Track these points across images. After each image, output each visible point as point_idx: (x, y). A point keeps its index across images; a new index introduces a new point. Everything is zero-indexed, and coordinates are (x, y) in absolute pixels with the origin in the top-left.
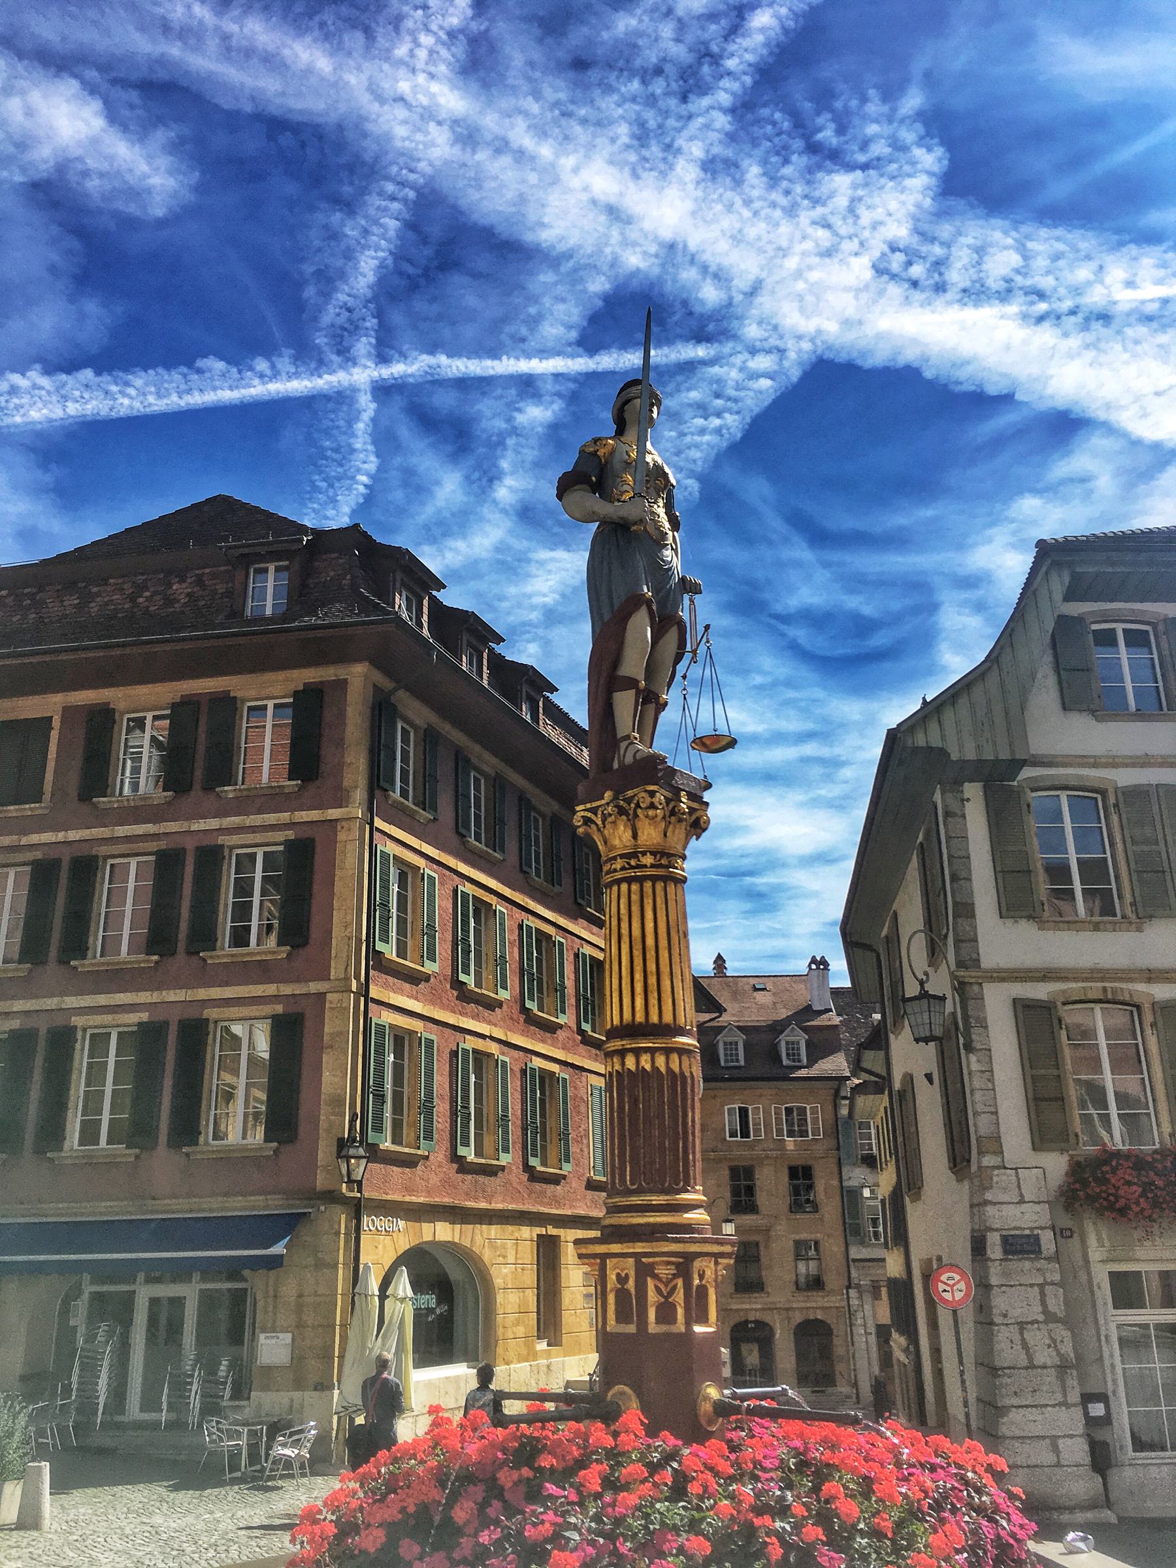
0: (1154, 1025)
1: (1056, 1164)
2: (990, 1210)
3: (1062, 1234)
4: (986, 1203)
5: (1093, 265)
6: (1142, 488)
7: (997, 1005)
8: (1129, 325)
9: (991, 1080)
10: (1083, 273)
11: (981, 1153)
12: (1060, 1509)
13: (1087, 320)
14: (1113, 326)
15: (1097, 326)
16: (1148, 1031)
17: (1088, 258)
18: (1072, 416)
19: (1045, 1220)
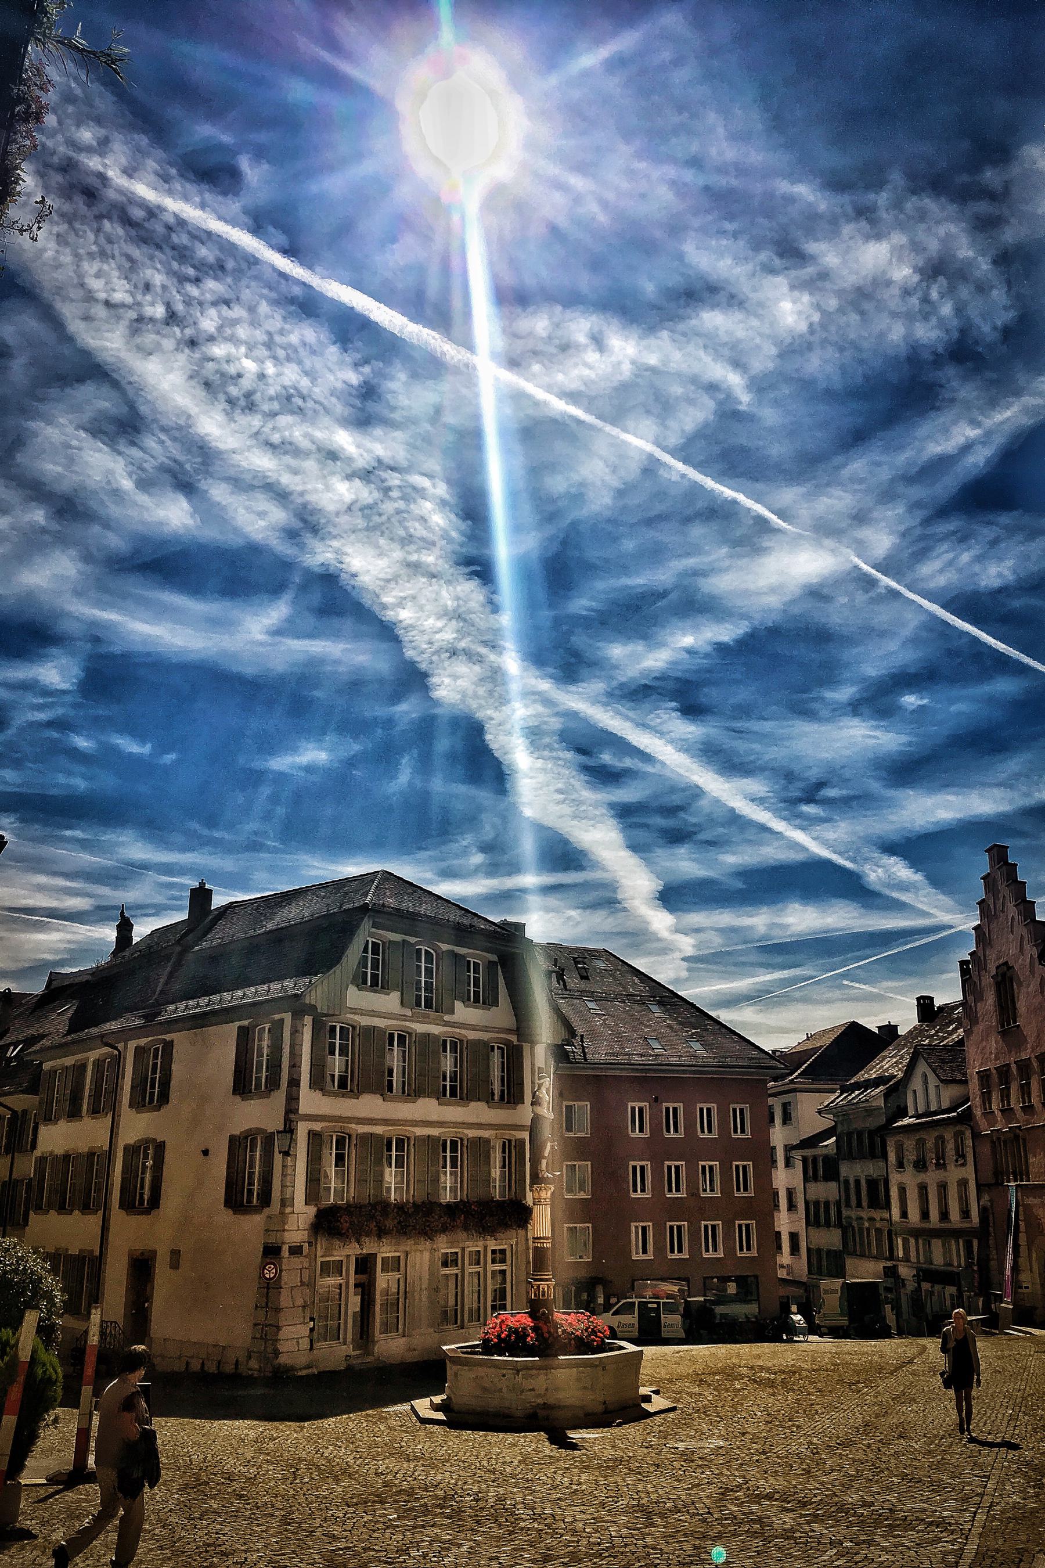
0: (356, 1145)
1: (312, 1210)
2: (286, 1233)
3: (310, 1243)
4: (284, 1230)
5: (102, 132)
6: (54, 392)
7: (302, 1129)
8: (110, 219)
9: (295, 1170)
10: (87, 135)
11: (951, 1265)
12: (296, 1370)
13: (72, 186)
14: (94, 208)
15: (80, 201)
16: (353, 1147)
17: (99, 121)
18: (19, 281)
19: (306, 1238)
